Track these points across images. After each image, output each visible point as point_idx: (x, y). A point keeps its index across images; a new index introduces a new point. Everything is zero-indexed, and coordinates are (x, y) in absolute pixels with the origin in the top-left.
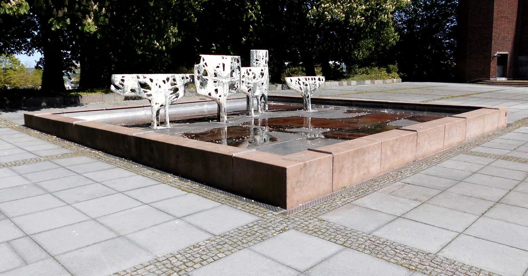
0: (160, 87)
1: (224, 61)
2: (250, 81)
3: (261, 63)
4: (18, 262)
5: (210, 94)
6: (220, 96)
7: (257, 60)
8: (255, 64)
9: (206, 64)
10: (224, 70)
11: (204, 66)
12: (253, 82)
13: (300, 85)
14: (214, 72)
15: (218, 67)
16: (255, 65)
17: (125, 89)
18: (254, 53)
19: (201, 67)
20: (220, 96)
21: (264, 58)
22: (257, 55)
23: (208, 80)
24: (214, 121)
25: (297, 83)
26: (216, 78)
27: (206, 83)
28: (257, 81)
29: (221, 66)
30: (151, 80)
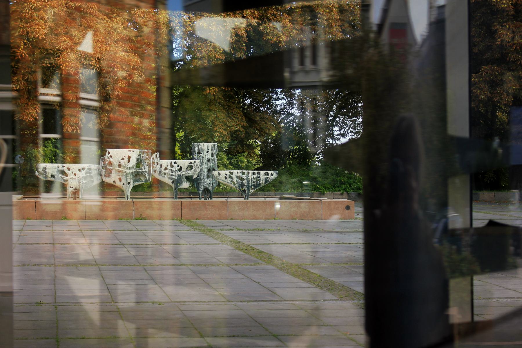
0: (75, 175)
1: (130, 154)
2: (174, 174)
3: (204, 156)
5: (114, 182)
6: (124, 184)
7: (199, 153)
8: (196, 157)
9: (111, 156)
11: (108, 158)
12: (176, 174)
13: (232, 178)
14: (118, 163)
15: (123, 159)
16: (197, 158)
17: (47, 175)
18: (195, 146)
19: (106, 159)
20: (124, 184)
21: (210, 151)
22: (200, 148)
23: (112, 170)
25: (228, 176)
26: (120, 169)
27: (111, 173)
28: (183, 173)
30: (69, 169)
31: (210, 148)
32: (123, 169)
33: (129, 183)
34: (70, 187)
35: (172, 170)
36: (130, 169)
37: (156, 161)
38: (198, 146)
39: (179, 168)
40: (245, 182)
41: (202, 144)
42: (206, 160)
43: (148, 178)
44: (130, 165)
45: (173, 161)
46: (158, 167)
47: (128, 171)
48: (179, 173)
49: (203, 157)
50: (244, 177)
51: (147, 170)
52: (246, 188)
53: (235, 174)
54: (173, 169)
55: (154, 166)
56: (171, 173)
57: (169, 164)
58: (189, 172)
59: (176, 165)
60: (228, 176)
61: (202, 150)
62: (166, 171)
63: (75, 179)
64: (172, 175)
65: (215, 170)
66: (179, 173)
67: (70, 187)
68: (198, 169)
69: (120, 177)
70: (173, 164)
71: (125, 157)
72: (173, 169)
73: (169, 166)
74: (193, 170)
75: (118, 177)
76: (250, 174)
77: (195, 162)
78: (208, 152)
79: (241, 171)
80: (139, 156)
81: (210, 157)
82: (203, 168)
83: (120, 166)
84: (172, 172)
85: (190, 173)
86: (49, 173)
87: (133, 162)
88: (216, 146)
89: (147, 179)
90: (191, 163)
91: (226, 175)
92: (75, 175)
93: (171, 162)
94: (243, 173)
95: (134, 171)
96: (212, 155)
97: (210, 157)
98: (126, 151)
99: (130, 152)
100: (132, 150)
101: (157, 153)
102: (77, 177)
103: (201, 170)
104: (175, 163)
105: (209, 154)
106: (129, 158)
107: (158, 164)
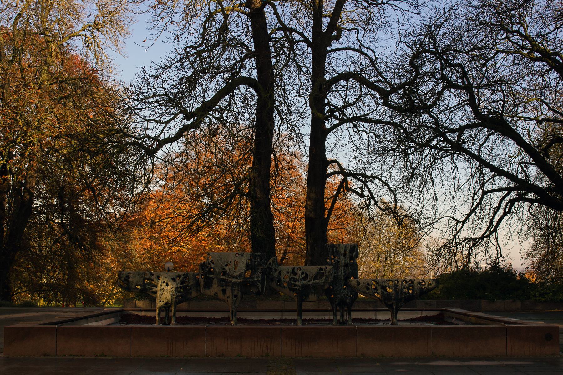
2: (297, 283)
28: (310, 283)
32: (228, 277)
34: (160, 301)
35: (294, 278)
36: (237, 278)
42: (343, 266)
43: (260, 289)
49: (339, 262)
51: (259, 279)
53: (380, 284)
54: (297, 277)
55: (272, 273)
58: (318, 281)
63: (167, 290)
67: (160, 301)
68: (330, 277)
69: (224, 288)
70: (295, 270)
71: (231, 262)
72: (297, 277)
77: (327, 268)
82: (338, 275)
84: (295, 281)
86: (133, 283)
89: (259, 291)
90: (321, 269)
93: (294, 269)
95: (242, 280)
103: (336, 278)
105: (347, 258)
107: (276, 270)
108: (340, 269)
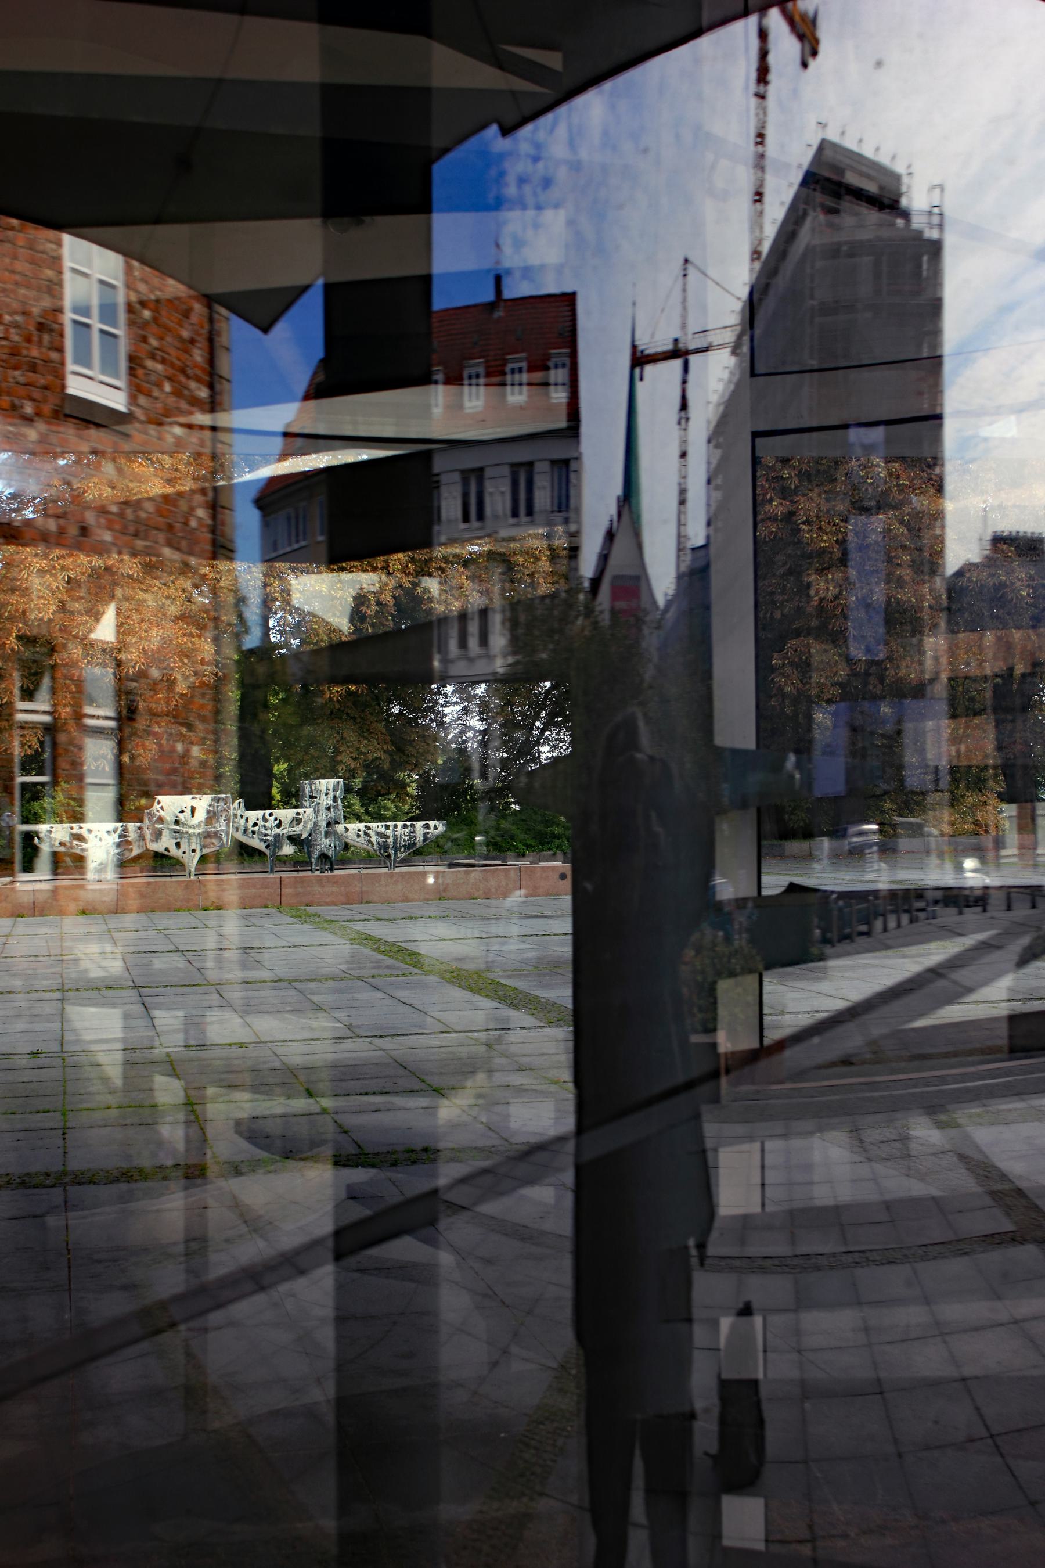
0: (101, 840)
1: (194, 803)
2: (268, 832)
3: (321, 802)
4: (677, 364)
6: (184, 853)
7: (311, 797)
9: (162, 808)
10: (193, 816)
12: (273, 833)
15: (182, 812)
20: (184, 853)
24: (787, 983)
25: (361, 833)
26: (177, 827)
28: (285, 831)
29: (188, 811)
31: (331, 788)
33: (194, 851)
35: (265, 826)
37: (239, 812)
38: (311, 784)
39: (277, 822)
40: (391, 841)
41: (317, 781)
44: (195, 821)
45: (268, 812)
46: (243, 821)
47: (191, 831)
48: (278, 831)
50: (389, 833)
52: (392, 852)
55: (236, 820)
56: (264, 831)
57: (261, 817)
59: (272, 818)
60: (361, 833)
61: (317, 791)
62: (256, 829)
63: (101, 847)
64: (266, 835)
65: (339, 823)
66: (278, 831)
69: (178, 841)
70: (267, 816)
73: (261, 820)
74: (302, 824)
75: (175, 841)
76: (399, 827)
78: (327, 794)
79: (384, 824)
80: (210, 805)
81: (330, 802)
83: (177, 822)
85: (297, 829)
87: (201, 815)
88: (341, 784)
90: (298, 814)
91: (359, 830)
92: (101, 840)
94: (387, 827)
96: (335, 799)
97: (330, 802)
98: (188, 797)
99: (195, 801)
100: (198, 796)
101: (240, 800)
102: (104, 843)
104: (271, 815)
106: (193, 810)
108: (321, 812)
